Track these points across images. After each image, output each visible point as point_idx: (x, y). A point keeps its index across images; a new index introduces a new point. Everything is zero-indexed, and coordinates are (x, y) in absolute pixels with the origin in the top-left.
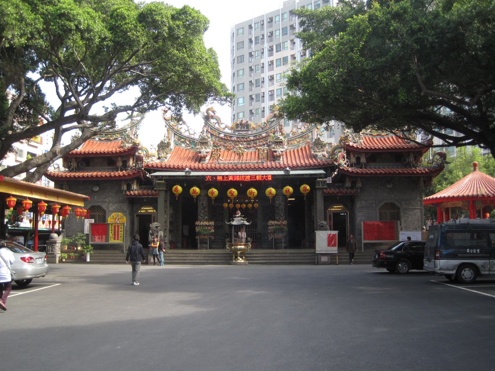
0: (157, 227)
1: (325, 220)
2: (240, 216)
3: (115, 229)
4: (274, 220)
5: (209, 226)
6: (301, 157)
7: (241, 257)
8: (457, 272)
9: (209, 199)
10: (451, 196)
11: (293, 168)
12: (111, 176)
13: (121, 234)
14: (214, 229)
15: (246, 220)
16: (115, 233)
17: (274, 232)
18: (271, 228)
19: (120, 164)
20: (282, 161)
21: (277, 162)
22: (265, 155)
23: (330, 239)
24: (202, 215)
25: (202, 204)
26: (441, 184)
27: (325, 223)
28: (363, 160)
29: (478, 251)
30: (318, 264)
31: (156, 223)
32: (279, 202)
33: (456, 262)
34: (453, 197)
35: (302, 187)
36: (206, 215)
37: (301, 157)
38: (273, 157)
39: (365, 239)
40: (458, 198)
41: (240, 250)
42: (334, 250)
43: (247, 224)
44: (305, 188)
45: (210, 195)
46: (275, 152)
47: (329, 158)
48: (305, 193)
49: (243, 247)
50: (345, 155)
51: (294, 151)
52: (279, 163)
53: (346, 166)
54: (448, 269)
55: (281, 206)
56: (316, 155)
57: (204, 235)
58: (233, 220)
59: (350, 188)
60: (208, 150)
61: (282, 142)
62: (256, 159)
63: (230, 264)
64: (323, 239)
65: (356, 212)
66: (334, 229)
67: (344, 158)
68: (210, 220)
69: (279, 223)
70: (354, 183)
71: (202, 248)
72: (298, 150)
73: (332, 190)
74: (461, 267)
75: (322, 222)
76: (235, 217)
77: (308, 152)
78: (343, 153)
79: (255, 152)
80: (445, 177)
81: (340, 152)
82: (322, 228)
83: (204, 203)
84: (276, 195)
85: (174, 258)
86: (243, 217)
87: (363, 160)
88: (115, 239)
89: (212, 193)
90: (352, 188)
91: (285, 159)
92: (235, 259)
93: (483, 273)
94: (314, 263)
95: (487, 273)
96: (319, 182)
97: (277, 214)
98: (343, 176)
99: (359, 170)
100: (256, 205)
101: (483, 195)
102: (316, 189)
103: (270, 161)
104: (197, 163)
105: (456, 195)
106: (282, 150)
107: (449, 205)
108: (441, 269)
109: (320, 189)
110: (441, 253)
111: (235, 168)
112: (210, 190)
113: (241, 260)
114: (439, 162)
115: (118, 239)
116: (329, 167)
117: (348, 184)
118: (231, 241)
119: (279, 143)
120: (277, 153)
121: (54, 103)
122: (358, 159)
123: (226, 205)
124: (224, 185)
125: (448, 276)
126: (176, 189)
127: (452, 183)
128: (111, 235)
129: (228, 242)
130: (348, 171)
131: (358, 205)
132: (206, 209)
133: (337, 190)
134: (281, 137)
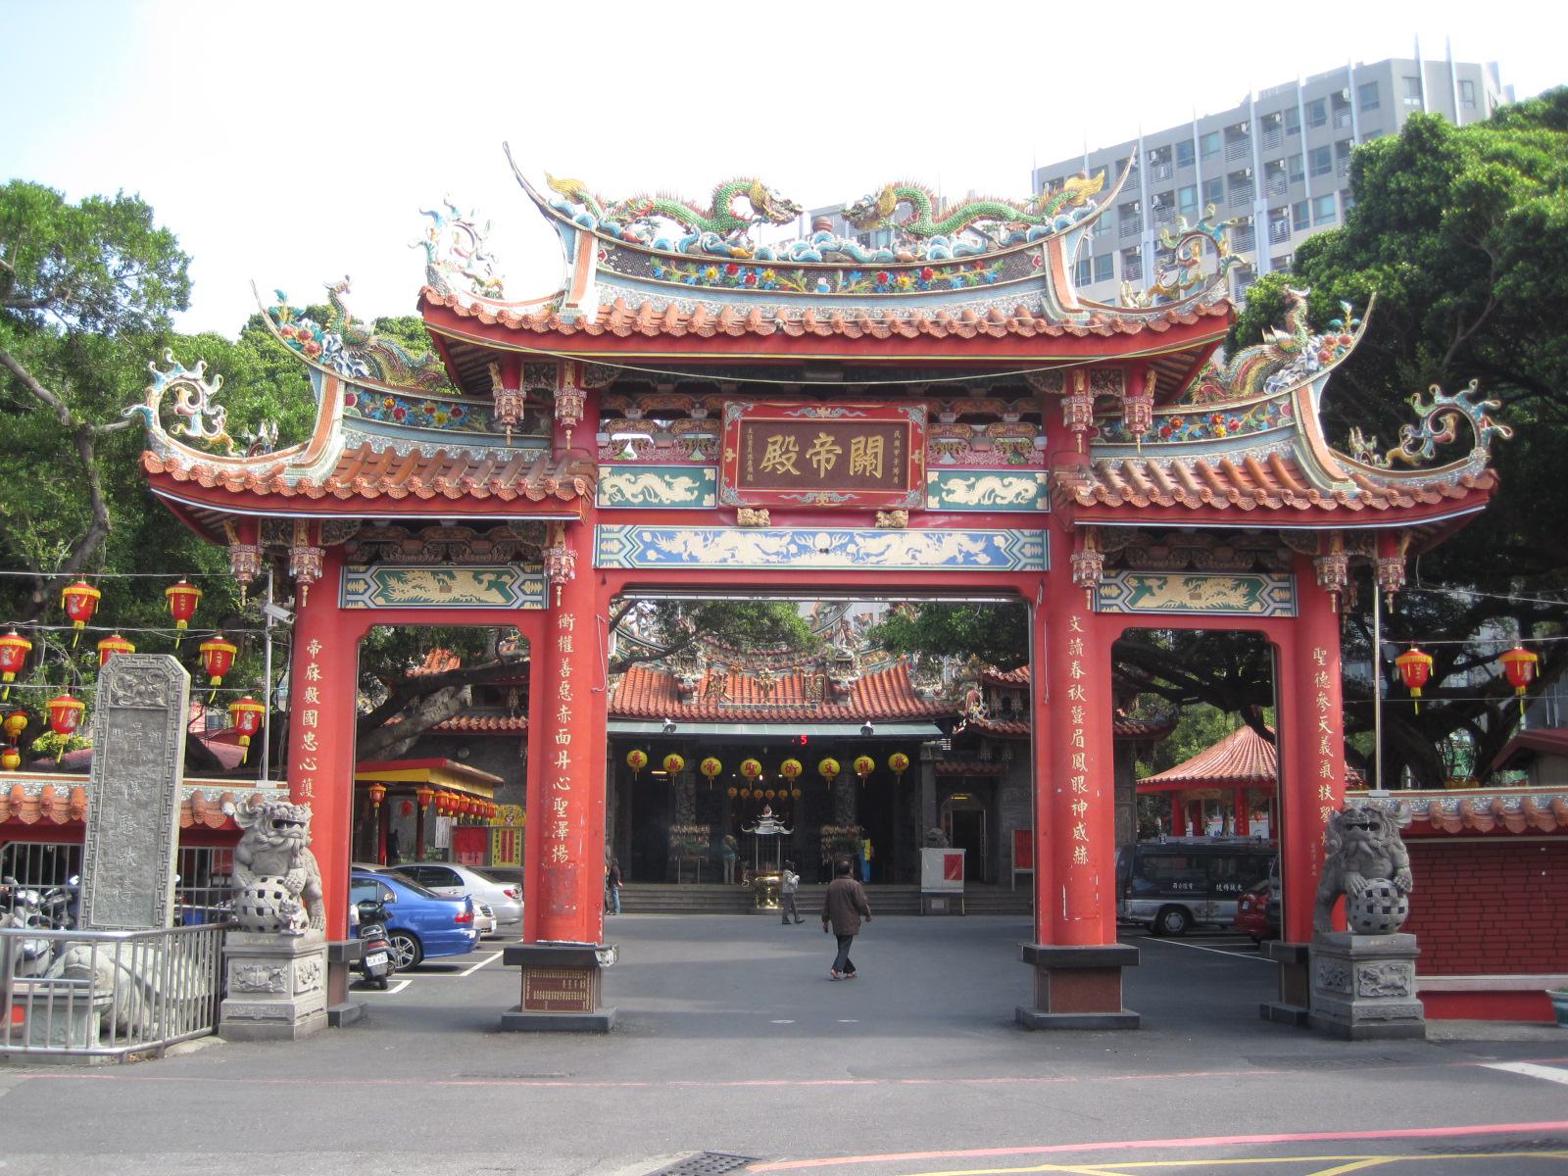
1: (938, 826)
3: (504, 840)
4: (833, 823)
5: (701, 834)
6: (890, 695)
7: (773, 900)
8: (1158, 917)
9: (701, 779)
10: (1197, 777)
11: (878, 720)
12: (499, 729)
13: (517, 849)
14: (710, 841)
16: (504, 846)
17: (833, 851)
18: (828, 840)
19: (513, 702)
20: (850, 704)
21: (841, 704)
22: (818, 691)
23: (950, 863)
26: (1188, 744)
27: (939, 832)
29: (1175, 885)
30: (925, 914)
32: (847, 792)
33: (1157, 903)
34: (1202, 780)
35: (893, 758)
37: (890, 695)
38: (832, 693)
39: (1017, 866)
40: (1212, 783)
41: (772, 884)
42: (957, 886)
43: (786, 832)
44: (899, 760)
45: (705, 771)
46: (838, 682)
48: (899, 771)
49: (776, 878)
50: (981, 695)
51: (872, 678)
52: (847, 709)
53: (980, 717)
54: (1144, 914)
56: (922, 693)
57: (691, 854)
58: (758, 825)
60: (698, 676)
61: (850, 663)
62: (798, 696)
63: (748, 913)
64: (935, 867)
66: (955, 846)
67: (978, 700)
68: (698, 823)
69: (844, 831)
71: (684, 880)
72: (881, 676)
73: (952, 767)
74: (1164, 911)
75: (934, 830)
77: (903, 682)
78: (977, 690)
79: (791, 679)
80: (1198, 727)
81: (971, 688)
82: (934, 843)
85: (632, 900)
88: (503, 860)
89: (711, 768)
90: (993, 761)
91: (856, 699)
93: (1198, 920)
94: (916, 912)
95: (1203, 920)
96: (926, 748)
98: (974, 738)
99: (1008, 727)
100: (796, 793)
101: (1260, 777)
102: (921, 763)
103: (827, 703)
105: (1207, 776)
106: (852, 679)
107: (1195, 794)
108: (1133, 913)
109: (928, 762)
110: (1133, 888)
111: (757, 716)
112: (706, 761)
113: (771, 906)
114: (1168, 712)
115: (511, 861)
116: (946, 719)
117: (986, 754)
118: (751, 867)
119: (846, 665)
120: (842, 686)
124: (734, 750)
125: (1147, 924)
126: (636, 758)
127: (1212, 743)
128: (495, 851)
130: (985, 728)
132: (693, 801)
133: (964, 766)
134: (850, 653)
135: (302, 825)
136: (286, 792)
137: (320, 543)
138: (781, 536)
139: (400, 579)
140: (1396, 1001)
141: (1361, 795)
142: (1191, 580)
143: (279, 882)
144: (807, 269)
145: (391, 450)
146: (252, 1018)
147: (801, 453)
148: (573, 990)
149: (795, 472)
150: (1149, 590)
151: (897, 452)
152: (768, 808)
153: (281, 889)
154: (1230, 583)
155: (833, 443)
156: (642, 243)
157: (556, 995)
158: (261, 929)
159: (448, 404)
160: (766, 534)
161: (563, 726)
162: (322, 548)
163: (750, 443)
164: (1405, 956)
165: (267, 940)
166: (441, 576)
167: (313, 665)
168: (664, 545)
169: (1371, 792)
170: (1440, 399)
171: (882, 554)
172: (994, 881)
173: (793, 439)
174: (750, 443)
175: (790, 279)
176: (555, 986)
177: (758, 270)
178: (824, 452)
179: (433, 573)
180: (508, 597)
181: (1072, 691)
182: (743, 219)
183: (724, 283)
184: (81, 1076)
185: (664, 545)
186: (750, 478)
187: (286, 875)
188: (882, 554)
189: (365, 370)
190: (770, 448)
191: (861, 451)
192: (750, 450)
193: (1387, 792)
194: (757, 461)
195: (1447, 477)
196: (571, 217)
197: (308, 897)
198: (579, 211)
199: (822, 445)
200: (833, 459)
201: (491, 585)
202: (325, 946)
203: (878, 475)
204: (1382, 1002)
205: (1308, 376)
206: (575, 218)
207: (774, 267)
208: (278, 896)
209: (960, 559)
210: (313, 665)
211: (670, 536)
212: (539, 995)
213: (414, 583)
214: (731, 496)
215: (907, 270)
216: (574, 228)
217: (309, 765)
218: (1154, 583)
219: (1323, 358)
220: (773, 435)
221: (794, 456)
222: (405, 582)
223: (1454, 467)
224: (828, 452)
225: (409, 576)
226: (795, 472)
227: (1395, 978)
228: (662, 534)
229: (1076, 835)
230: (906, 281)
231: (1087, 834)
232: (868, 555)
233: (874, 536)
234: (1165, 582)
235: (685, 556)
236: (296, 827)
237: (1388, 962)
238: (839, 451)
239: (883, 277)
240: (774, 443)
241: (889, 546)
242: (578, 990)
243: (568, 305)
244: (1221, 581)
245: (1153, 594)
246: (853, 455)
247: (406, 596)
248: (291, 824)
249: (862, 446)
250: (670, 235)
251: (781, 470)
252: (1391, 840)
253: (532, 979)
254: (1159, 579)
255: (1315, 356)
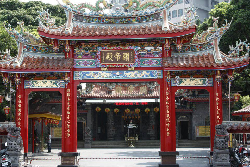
0: (89, 129)
2: (132, 123)
7: (133, 145)
9: (114, 113)
15: (135, 125)
24: (110, 122)
25: (111, 116)
28: (197, 93)
31: (88, 127)
36: (113, 122)
41: (132, 140)
45: (115, 112)
46: (150, 88)
47: (178, 92)
55: (153, 117)
59: (189, 108)
65: (193, 121)
70: (191, 106)
76: (130, 124)
83: (112, 116)
84: (150, 111)
86: (134, 124)
87: (197, 93)
90: (190, 108)
92: (130, 145)
97: (151, 122)
104: (17, 63)
120: (151, 89)
121: (7, 45)
122: (194, 92)
123: (123, 117)
129: (126, 136)
131: (194, 117)
135: (19, 131)
136: (15, 124)
137: (20, 77)
138: (110, 73)
139: (36, 83)
140: (225, 162)
141: (225, 122)
142: (191, 79)
143: (15, 142)
144: (114, 18)
145: (33, 57)
146: (172, 6)
147: (113, 56)
148: (71, 161)
149: (112, 60)
150: (183, 82)
151: (132, 56)
152: (131, 121)
153: (15, 143)
154: (199, 80)
155: (119, 54)
156: (81, 14)
157: (68, 162)
158: (12, 150)
159: (44, 48)
160: (107, 72)
161: (68, 111)
162: (21, 78)
163: (103, 55)
164: (227, 153)
165: (14, 152)
166: (44, 82)
167: (20, 100)
168: (87, 75)
169: (227, 122)
170: (241, 43)
171: (130, 76)
172: (191, 139)
173: (111, 54)
174: (103, 55)
175: (111, 20)
176: (68, 160)
177: (105, 19)
178: (118, 56)
179: (43, 81)
180: (57, 86)
181: (166, 102)
182: (101, 8)
183: (98, 22)
184: (166, 54)
185: (87, 75)
186: (103, 61)
187: (16, 140)
188: (130, 76)
189: (27, 41)
190: (107, 56)
191: (125, 56)
192: (103, 56)
193: (230, 122)
194: (105, 58)
195: (241, 59)
196: (67, 8)
197: (20, 144)
198: (69, 7)
199: (117, 55)
200: (120, 57)
201: (54, 83)
202: (24, 153)
203: (128, 60)
204: (222, 162)
205: (217, 37)
206: (68, 9)
207: (108, 18)
208: (15, 144)
209: (145, 76)
210: (20, 100)
211: (88, 73)
212: (65, 162)
213: (39, 83)
214: (99, 65)
215: (134, 18)
216: (68, 11)
217: (20, 119)
218: (183, 80)
219: (220, 33)
220: (107, 53)
221: (112, 57)
222: (37, 83)
223: (242, 57)
224: (118, 56)
225: (38, 82)
226: (112, 60)
227: (225, 158)
228: (87, 73)
229: (167, 130)
230: (134, 20)
231: (169, 130)
232: (127, 76)
233: (128, 72)
234: (186, 80)
235: (91, 77)
236: (18, 132)
237: (224, 155)
238: (120, 56)
239: (129, 20)
240: (108, 55)
241: (131, 74)
242: (72, 161)
243: (67, 30)
244: (197, 80)
245: (183, 82)
246: (123, 57)
247: (38, 86)
248: (17, 131)
249: (125, 55)
250: (87, 11)
251: (109, 60)
252: (224, 131)
253: (63, 159)
254: (184, 79)
255: (218, 32)
